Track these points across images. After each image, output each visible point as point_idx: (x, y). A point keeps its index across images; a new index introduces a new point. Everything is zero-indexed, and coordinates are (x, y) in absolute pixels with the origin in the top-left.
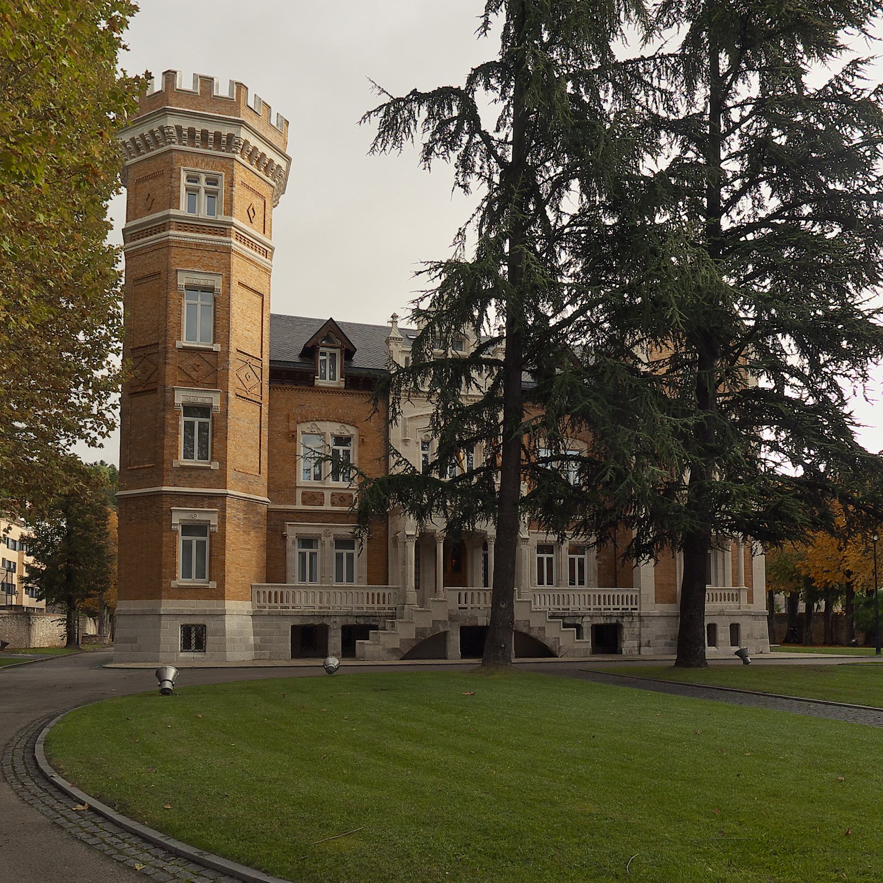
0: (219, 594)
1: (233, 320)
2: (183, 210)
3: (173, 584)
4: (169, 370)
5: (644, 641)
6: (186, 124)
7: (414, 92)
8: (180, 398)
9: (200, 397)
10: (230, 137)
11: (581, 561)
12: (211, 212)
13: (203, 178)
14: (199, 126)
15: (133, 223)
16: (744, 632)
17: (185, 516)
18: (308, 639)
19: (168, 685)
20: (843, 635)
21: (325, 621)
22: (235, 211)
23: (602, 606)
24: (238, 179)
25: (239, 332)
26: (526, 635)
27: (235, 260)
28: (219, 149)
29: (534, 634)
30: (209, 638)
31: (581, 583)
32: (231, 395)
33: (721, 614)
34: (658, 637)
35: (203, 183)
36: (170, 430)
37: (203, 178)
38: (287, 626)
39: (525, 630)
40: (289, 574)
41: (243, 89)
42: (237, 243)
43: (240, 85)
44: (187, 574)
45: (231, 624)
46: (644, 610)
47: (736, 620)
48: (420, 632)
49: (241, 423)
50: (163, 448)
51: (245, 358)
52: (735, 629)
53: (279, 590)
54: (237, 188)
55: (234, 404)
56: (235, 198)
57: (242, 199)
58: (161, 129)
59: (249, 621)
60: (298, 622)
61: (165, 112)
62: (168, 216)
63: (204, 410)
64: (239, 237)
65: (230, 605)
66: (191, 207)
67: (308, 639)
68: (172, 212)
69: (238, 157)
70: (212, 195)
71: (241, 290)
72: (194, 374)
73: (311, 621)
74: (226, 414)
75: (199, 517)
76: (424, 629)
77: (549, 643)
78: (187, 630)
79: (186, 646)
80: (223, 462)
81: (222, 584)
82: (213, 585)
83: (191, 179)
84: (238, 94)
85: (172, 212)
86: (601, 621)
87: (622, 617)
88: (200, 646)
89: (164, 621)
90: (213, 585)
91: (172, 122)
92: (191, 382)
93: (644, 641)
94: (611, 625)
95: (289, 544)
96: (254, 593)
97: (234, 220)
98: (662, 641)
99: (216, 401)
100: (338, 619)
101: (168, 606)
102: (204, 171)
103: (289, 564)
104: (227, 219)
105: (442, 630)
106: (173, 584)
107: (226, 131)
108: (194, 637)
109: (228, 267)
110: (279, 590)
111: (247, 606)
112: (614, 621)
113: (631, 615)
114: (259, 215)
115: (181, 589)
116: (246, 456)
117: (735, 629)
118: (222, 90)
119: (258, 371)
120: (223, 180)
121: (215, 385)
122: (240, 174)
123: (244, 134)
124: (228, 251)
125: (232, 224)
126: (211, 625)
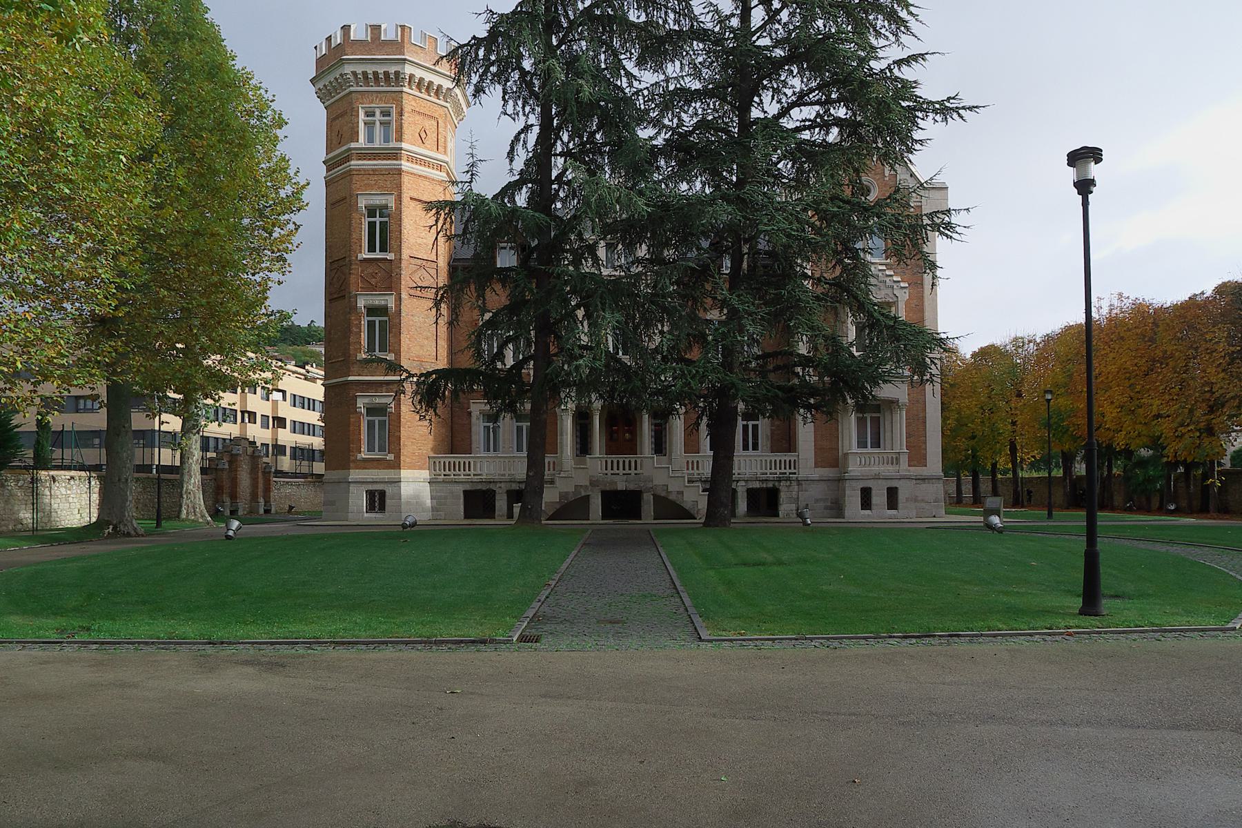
0: (396, 465)
1: (404, 231)
2: (362, 141)
3: (359, 456)
4: (353, 279)
5: (802, 504)
6: (359, 69)
7: (474, 38)
8: (361, 303)
9: (377, 301)
10: (397, 73)
11: (755, 427)
12: (387, 140)
13: (378, 112)
14: (370, 69)
15: (331, 155)
16: (902, 496)
17: (366, 400)
18: (479, 501)
19: (231, 533)
20: (1155, 503)
21: (492, 486)
22: (405, 137)
23: (769, 471)
24: (407, 108)
25: (412, 240)
26: (665, 499)
27: (405, 179)
28: (389, 85)
29: (672, 497)
30: (388, 502)
31: (755, 447)
32: (404, 295)
33: (877, 477)
34: (817, 501)
35: (378, 116)
36: (355, 329)
37: (378, 112)
38: (459, 489)
39: (663, 494)
40: (474, 446)
41: (407, 30)
42: (409, 164)
43: (403, 27)
44: (371, 449)
45: (406, 490)
46: (803, 474)
47: (894, 484)
48: (563, 495)
49: (416, 319)
50: (349, 344)
51: (419, 262)
52: (892, 494)
53: (452, 461)
54: (406, 115)
55: (408, 305)
56: (405, 126)
57: (411, 124)
58: (341, 75)
59: (427, 487)
60: (468, 487)
61: (342, 62)
62: (350, 149)
63: (381, 311)
64: (411, 159)
65: (405, 473)
66: (370, 139)
67: (479, 501)
68: (353, 145)
69: (405, 89)
70: (385, 124)
71: (413, 203)
72: (373, 281)
73: (479, 487)
74: (399, 312)
75: (378, 400)
76: (567, 493)
77: (687, 506)
78: (371, 494)
79: (371, 508)
80: (398, 354)
81: (398, 456)
82: (391, 457)
83: (370, 114)
84: (403, 35)
85: (353, 145)
86: (757, 485)
87: (780, 481)
88: (382, 508)
89: (352, 487)
90: (391, 457)
91: (348, 69)
92: (371, 288)
93: (802, 504)
94: (768, 489)
95: (474, 419)
96: (433, 464)
97: (404, 145)
98: (822, 504)
99: (391, 302)
100: (503, 485)
101: (355, 474)
102: (378, 106)
103: (474, 438)
104: (397, 145)
105: (583, 494)
106: (359, 456)
107: (392, 69)
108: (377, 500)
109: (399, 187)
110: (452, 461)
111: (425, 474)
112: (770, 485)
113: (788, 479)
114: (432, 136)
115: (365, 460)
116: (422, 346)
117: (892, 494)
118: (388, 33)
119: (433, 272)
120: (394, 112)
121: (390, 289)
122: (408, 104)
123: (408, 70)
124: (399, 172)
125: (401, 149)
126: (389, 490)
